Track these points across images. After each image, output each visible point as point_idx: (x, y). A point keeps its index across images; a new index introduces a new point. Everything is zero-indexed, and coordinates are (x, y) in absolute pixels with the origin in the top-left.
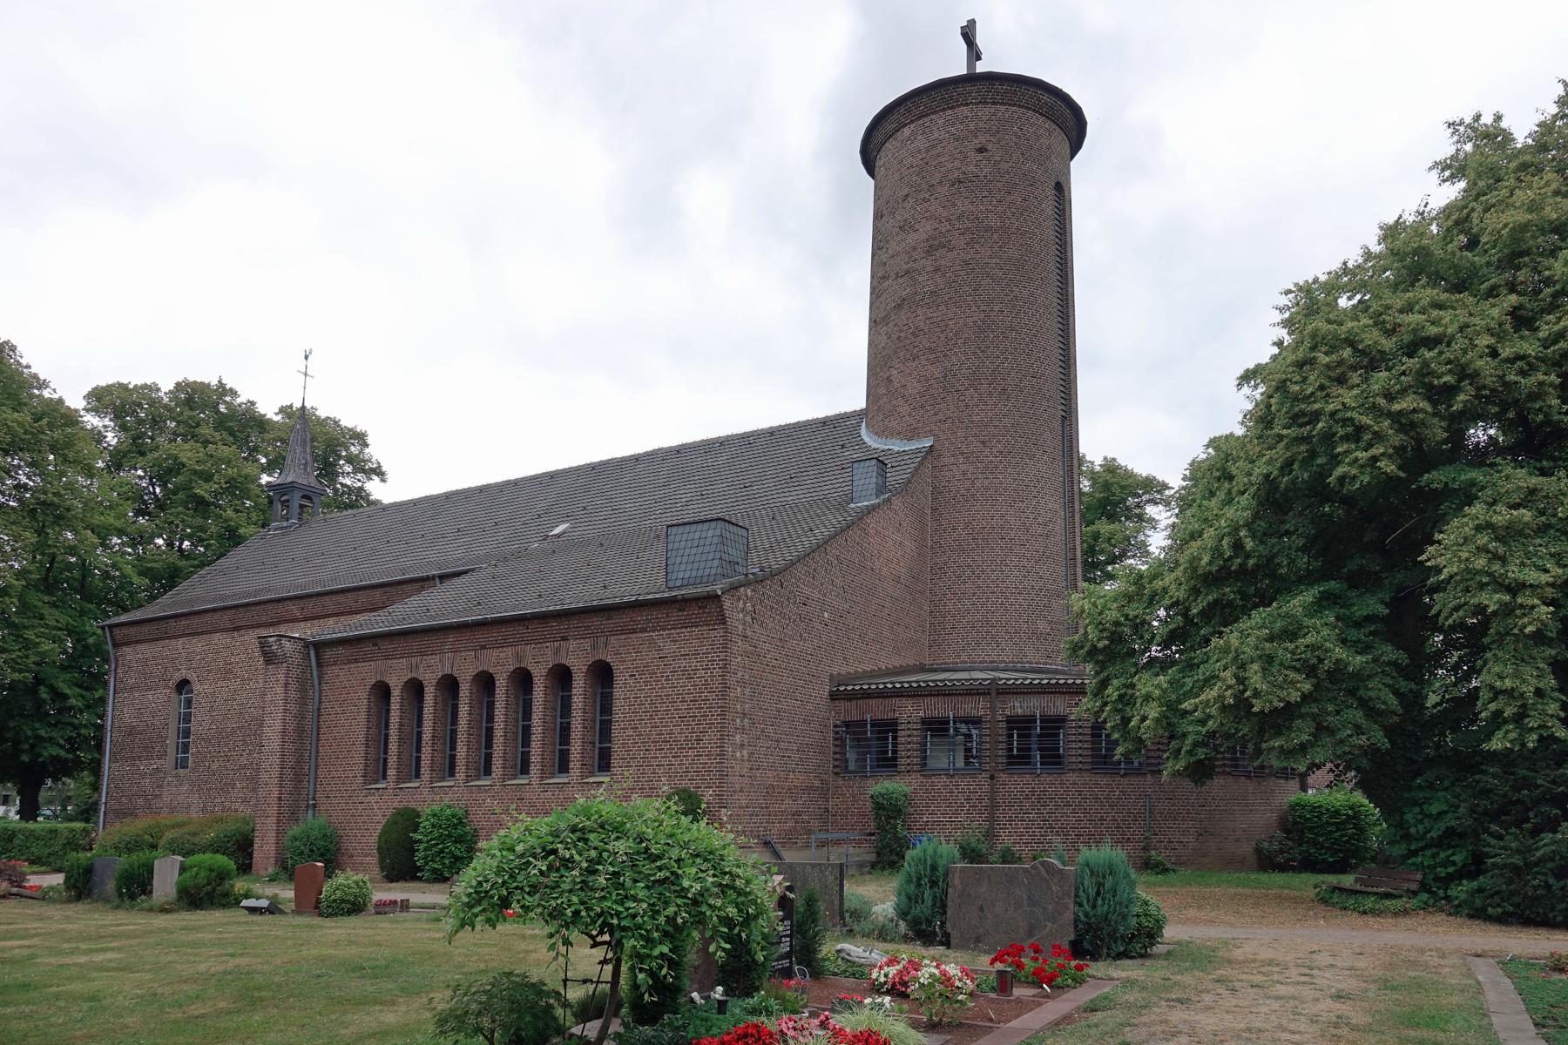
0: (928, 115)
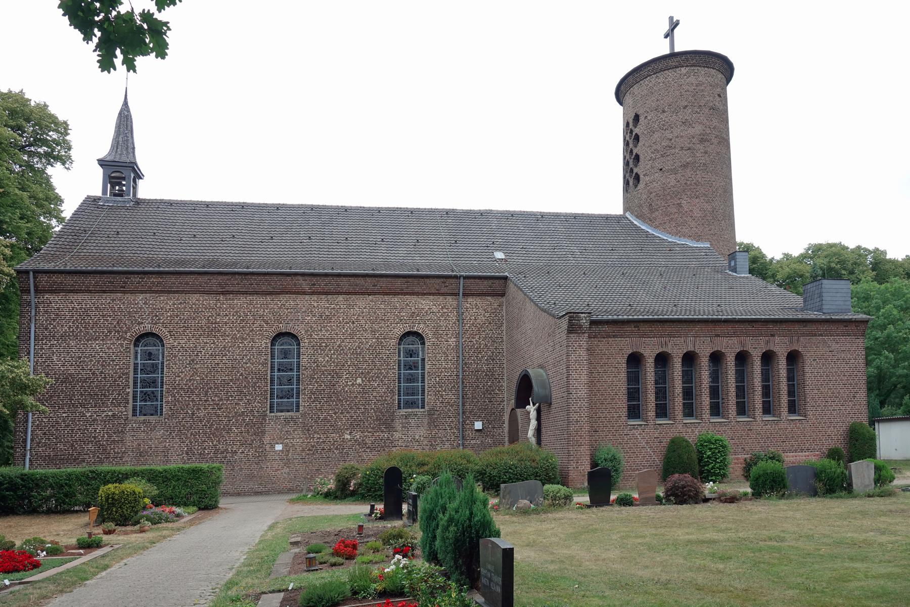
0: (696, 66)
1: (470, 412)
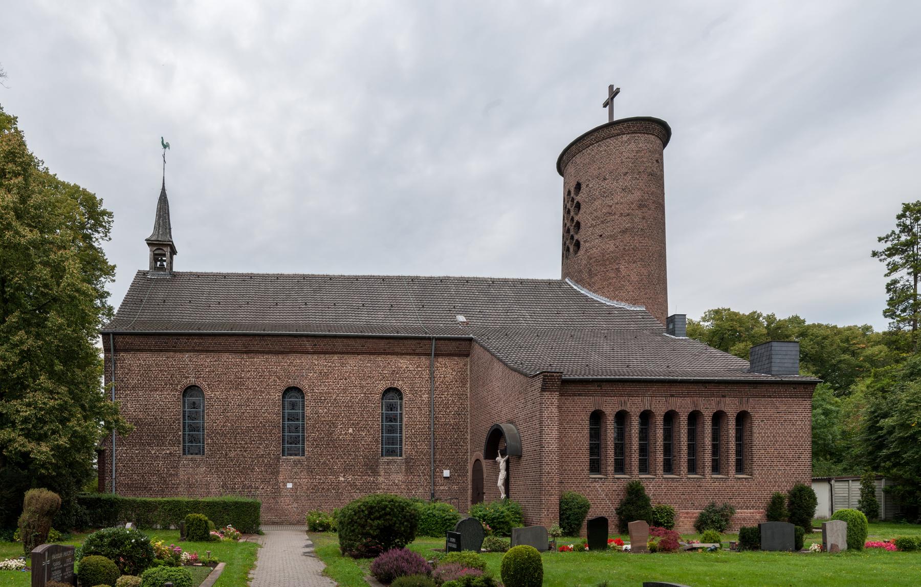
0: (637, 133)
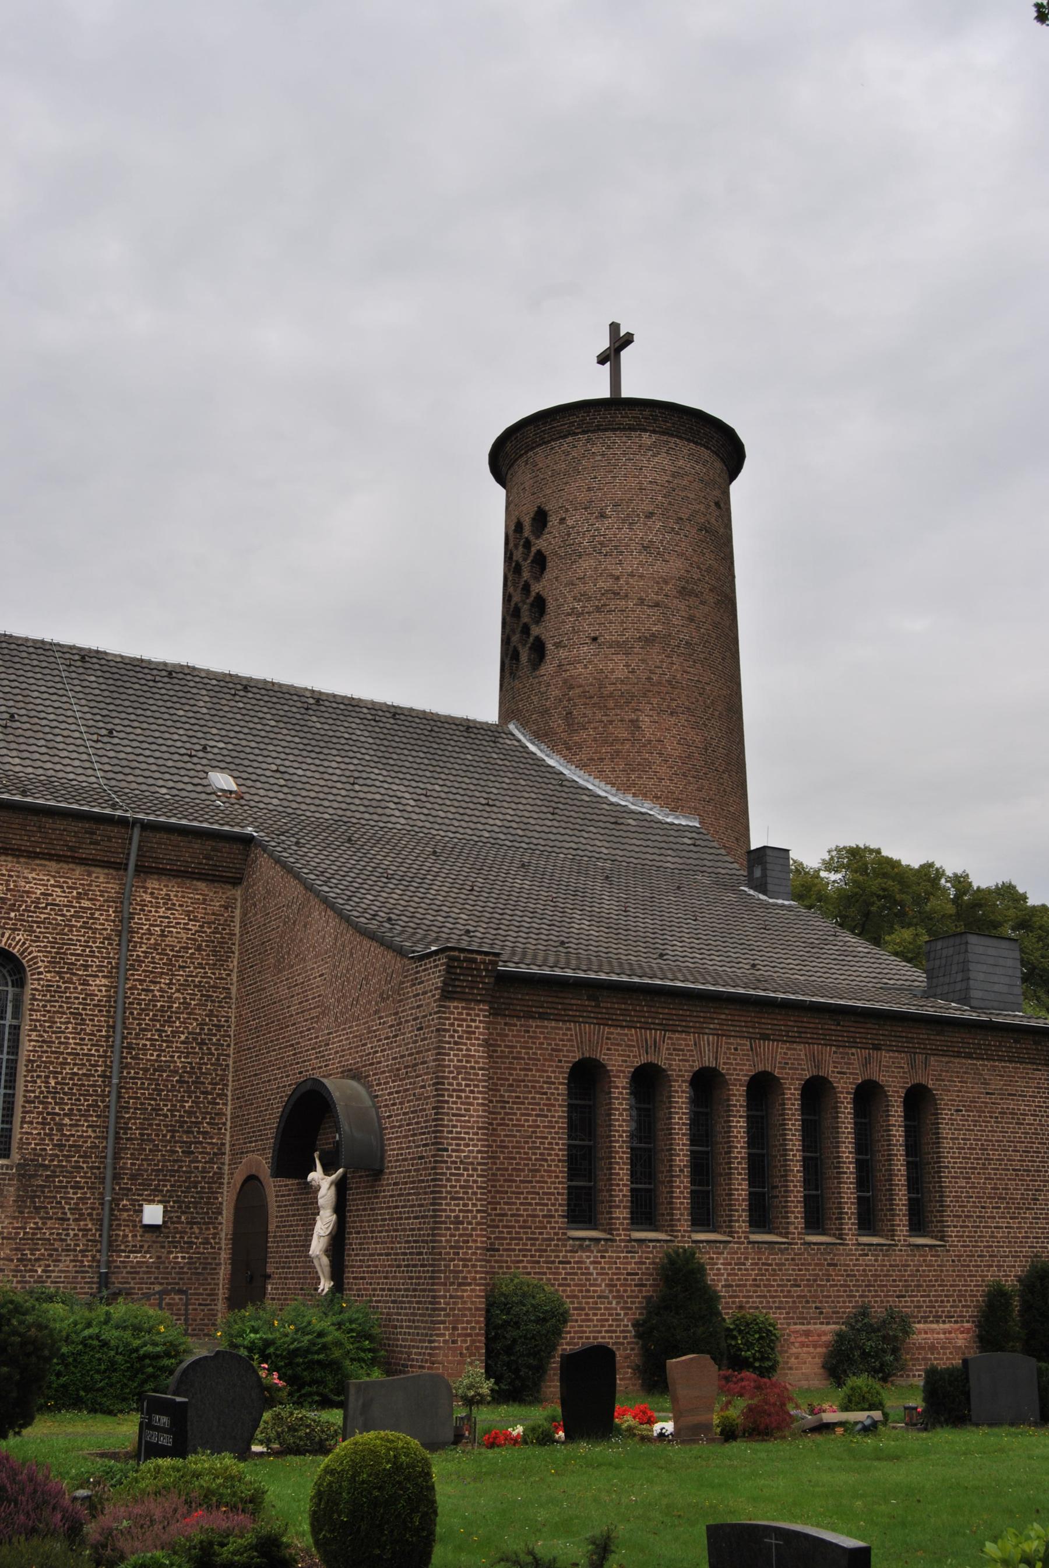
0: (672, 435)
1: (133, 1177)
